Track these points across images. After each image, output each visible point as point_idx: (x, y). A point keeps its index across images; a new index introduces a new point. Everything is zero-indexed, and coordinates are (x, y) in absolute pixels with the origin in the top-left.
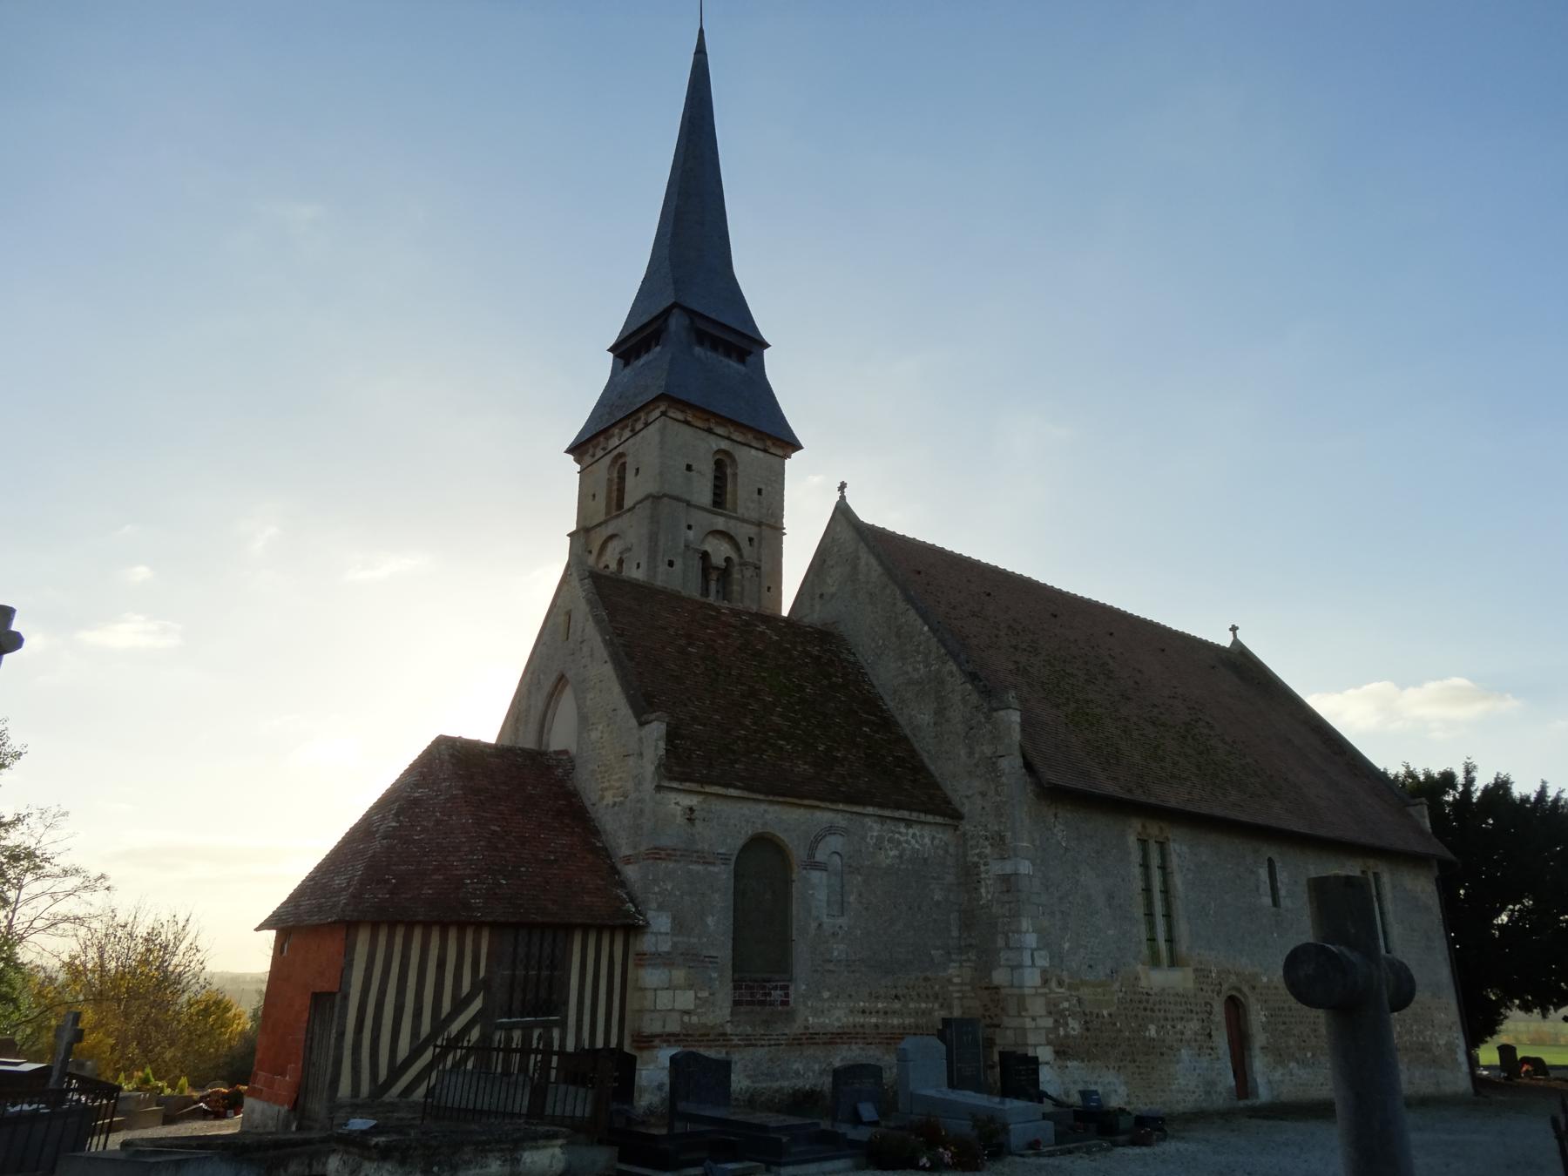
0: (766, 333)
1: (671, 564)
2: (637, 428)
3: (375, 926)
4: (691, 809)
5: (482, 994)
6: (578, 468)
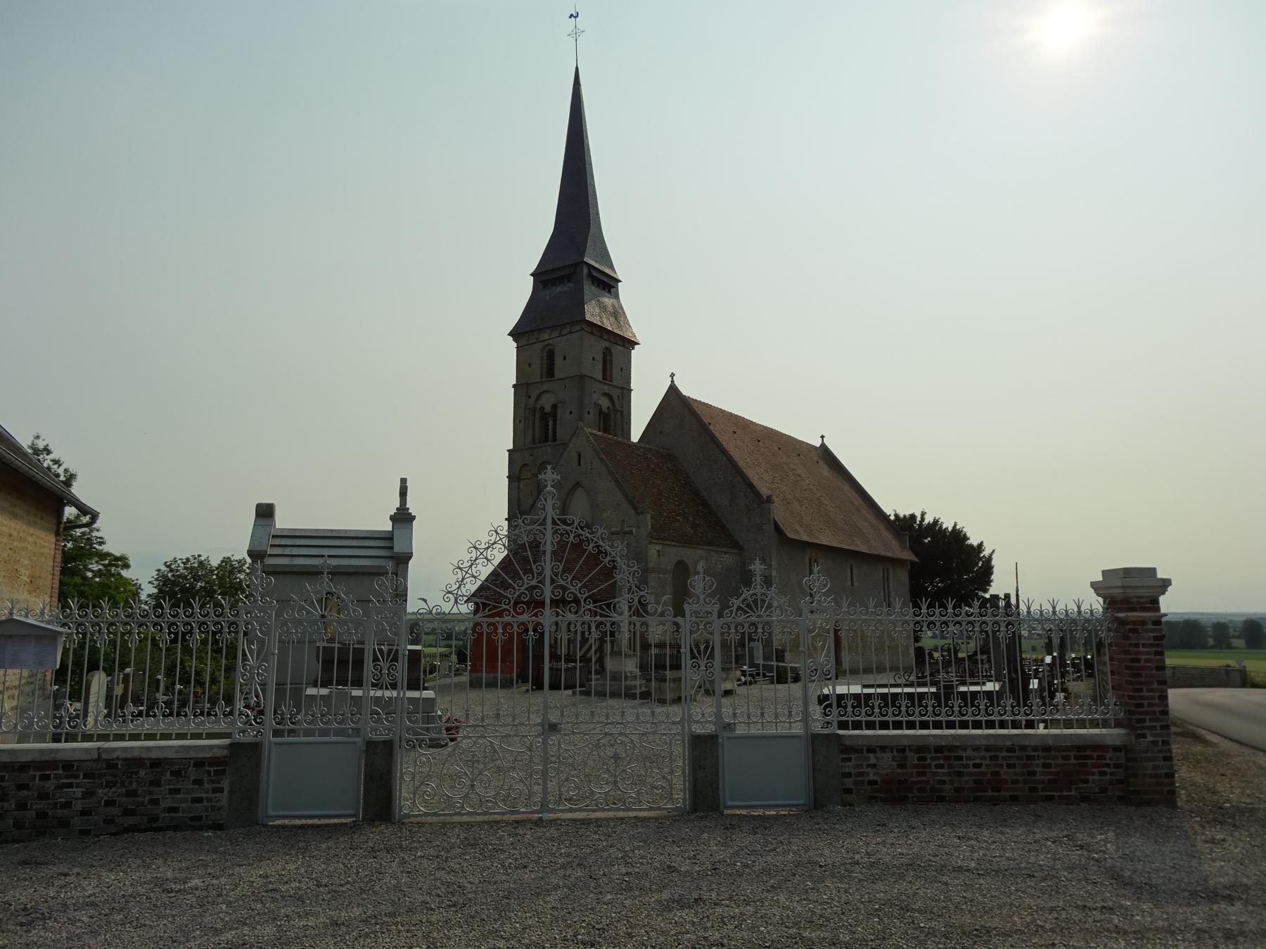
2: (563, 334)
4: (659, 551)
6: (515, 345)
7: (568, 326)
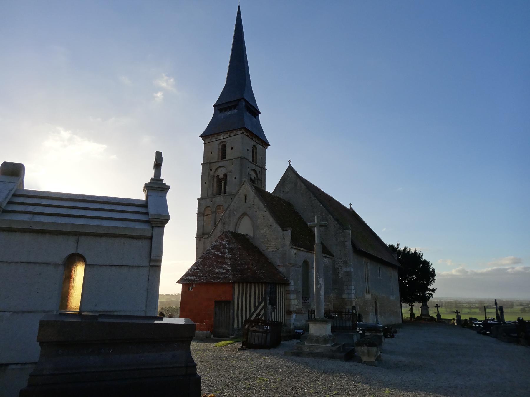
0: (260, 110)
1: (235, 178)
3: (239, 283)
4: (295, 253)
6: (204, 142)
7: (235, 132)
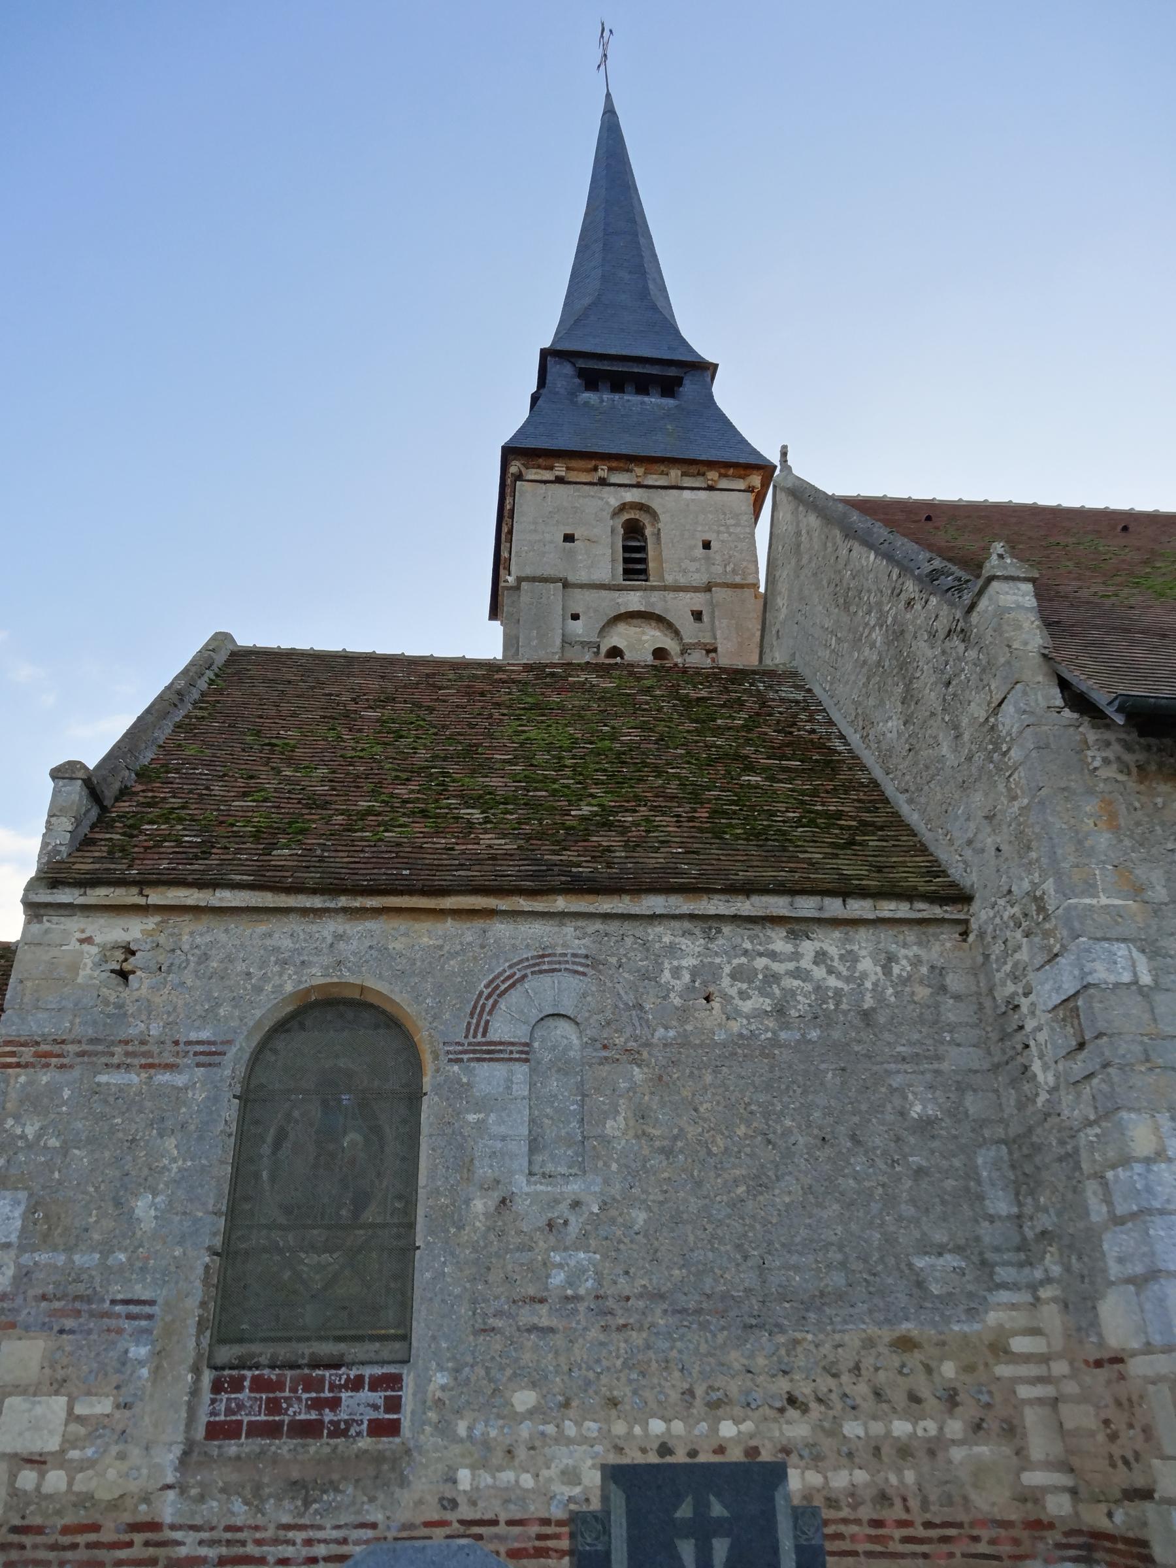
5: (712, 1498)
